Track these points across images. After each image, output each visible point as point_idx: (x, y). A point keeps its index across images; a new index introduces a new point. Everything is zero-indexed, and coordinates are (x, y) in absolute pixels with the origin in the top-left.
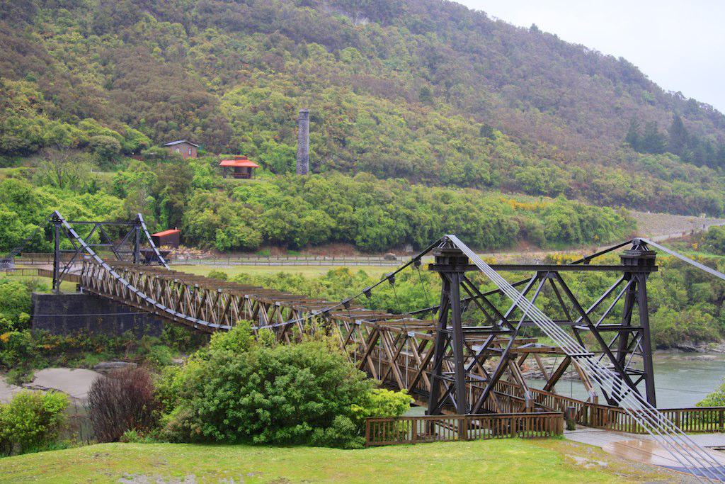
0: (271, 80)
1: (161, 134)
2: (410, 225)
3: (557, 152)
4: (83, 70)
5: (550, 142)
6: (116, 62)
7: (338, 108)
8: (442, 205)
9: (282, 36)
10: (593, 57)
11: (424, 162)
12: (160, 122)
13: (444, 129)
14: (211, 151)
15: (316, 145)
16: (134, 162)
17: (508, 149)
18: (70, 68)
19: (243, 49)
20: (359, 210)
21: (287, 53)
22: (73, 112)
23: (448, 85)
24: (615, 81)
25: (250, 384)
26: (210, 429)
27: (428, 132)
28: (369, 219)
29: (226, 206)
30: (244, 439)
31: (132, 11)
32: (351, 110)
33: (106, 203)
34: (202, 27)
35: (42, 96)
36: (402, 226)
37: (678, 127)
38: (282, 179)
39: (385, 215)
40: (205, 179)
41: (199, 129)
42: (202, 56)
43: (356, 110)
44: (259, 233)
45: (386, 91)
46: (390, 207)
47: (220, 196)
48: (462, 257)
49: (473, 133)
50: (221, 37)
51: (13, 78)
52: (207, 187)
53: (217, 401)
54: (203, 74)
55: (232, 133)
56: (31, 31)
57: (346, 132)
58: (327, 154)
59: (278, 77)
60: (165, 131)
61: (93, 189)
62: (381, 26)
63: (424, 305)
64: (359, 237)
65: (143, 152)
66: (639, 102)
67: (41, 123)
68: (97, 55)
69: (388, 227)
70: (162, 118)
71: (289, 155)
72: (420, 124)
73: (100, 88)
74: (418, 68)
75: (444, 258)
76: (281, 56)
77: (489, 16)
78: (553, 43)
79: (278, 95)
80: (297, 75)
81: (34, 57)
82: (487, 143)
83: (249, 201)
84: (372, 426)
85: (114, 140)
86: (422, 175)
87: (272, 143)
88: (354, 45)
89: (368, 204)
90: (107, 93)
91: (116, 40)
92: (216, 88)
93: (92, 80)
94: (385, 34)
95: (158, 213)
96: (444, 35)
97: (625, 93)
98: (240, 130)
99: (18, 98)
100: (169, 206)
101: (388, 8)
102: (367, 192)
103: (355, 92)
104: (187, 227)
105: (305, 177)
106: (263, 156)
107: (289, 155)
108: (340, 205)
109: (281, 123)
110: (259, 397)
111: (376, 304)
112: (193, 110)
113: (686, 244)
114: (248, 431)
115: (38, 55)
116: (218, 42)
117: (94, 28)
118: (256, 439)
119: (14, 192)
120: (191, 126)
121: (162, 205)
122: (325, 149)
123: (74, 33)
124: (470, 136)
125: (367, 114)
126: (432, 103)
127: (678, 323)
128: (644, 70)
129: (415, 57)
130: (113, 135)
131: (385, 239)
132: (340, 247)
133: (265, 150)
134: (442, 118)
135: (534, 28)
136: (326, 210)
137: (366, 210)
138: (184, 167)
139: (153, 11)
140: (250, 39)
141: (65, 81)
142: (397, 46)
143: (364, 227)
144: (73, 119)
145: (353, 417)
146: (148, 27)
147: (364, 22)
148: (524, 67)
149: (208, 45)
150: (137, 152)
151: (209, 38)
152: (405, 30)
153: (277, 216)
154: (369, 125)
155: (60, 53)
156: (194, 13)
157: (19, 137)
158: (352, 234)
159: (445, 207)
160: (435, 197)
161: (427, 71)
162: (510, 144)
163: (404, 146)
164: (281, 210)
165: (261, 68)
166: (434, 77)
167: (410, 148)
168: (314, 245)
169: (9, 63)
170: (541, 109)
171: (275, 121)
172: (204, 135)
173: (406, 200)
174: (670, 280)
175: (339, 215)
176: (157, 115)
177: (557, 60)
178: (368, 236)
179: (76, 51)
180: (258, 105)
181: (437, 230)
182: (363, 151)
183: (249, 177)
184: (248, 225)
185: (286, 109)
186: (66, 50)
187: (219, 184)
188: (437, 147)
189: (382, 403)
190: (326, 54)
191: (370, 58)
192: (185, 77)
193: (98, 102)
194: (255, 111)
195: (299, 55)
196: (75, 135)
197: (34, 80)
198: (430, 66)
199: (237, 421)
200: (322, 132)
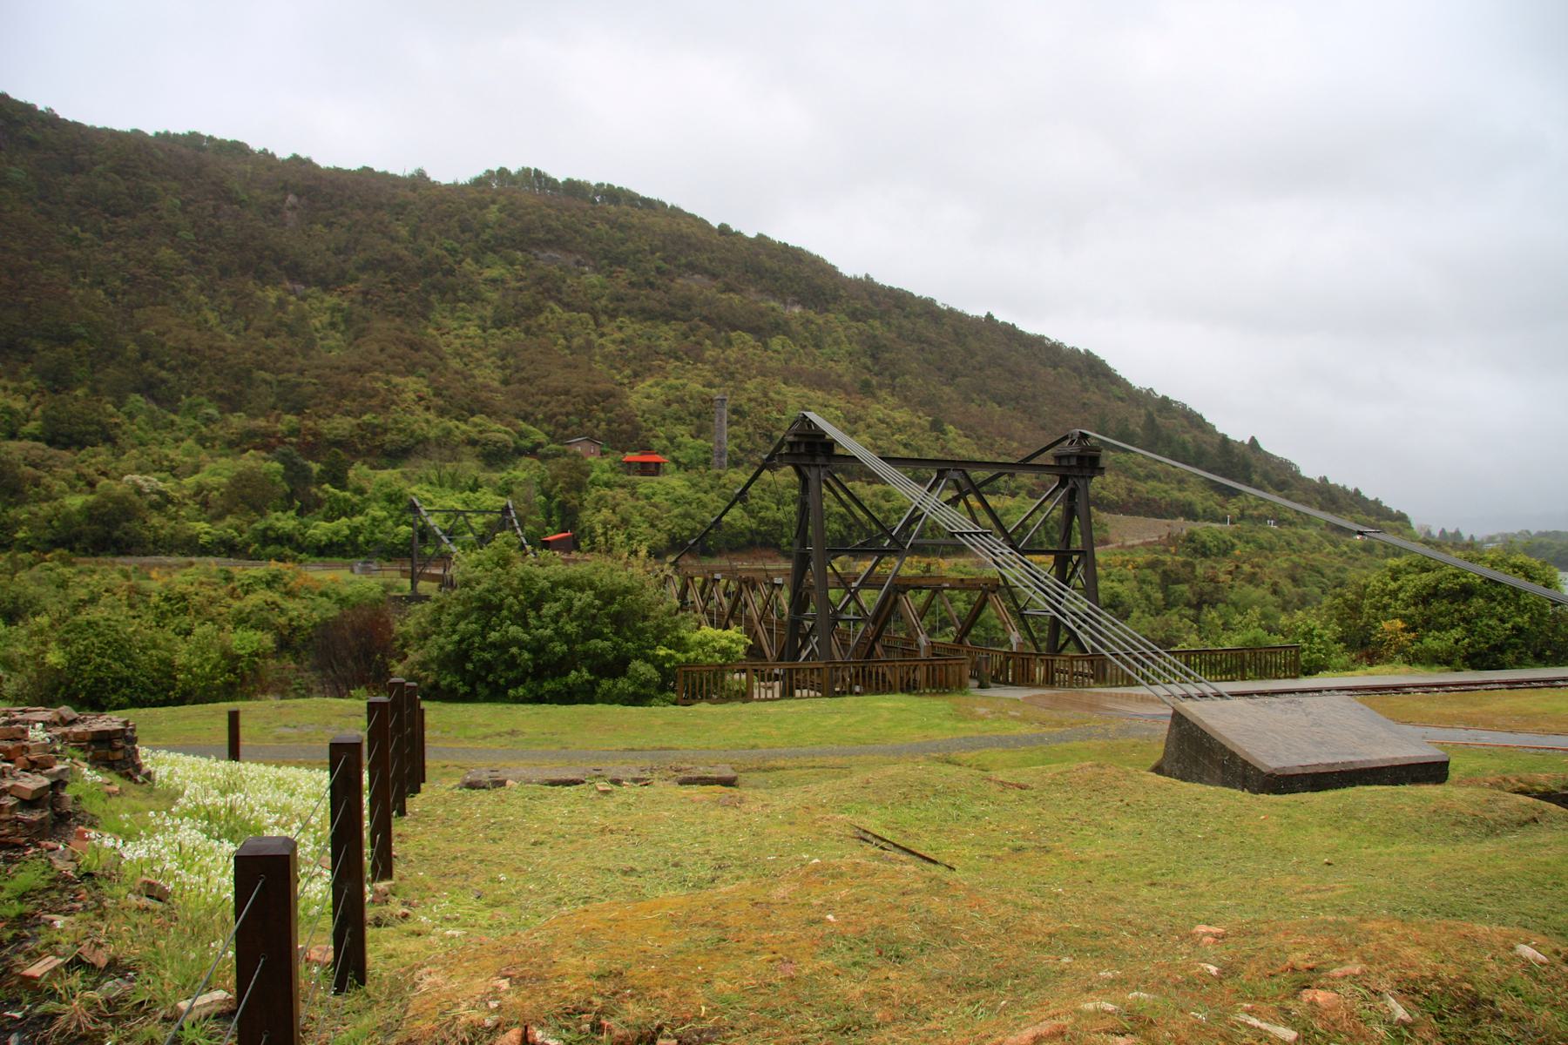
0: (688, 371)
1: (560, 431)
3: (1018, 449)
4: (478, 366)
5: (1010, 438)
6: (515, 355)
7: (764, 400)
8: (882, 503)
9: (702, 324)
10: (1056, 349)
12: (559, 417)
13: (887, 423)
14: (617, 449)
15: (738, 441)
16: (526, 460)
17: (962, 446)
18: (466, 365)
19: (659, 338)
22: (462, 408)
23: (893, 377)
24: (1081, 375)
25: (505, 613)
26: (449, 679)
27: (869, 426)
29: (627, 504)
30: (497, 694)
31: (536, 302)
32: (779, 401)
33: (489, 502)
34: (613, 316)
37: (1150, 423)
38: (693, 475)
40: (605, 477)
41: (603, 425)
42: (611, 348)
43: (785, 402)
44: (665, 536)
45: (820, 381)
47: (620, 494)
48: (822, 444)
49: (922, 428)
50: (632, 327)
51: (402, 375)
52: (607, 485)
53: (456, 637)
54: (611, 367)
55: (641, 428)
56: (426, 327)
58: (752, 451)
60: (566, 427)
61: (475, 487)
65: (539, 450)
66: (1108, 399)
67: (428, 421)
68: (496, 349)
70: (561, 414)
71: (706, 452)
72: (859, 418)
73: (496, 384)
75: (798, 444)
77: (939, 303)
78: (1010, 332)
79: (696, 387)
80: (718, 365)
81: (426, 353)
82: (938, 439)
83: (656, 499)
84: (687, 676)
85: (506, 437)
87: (687, 439)
88: (785, 334)
90: (503, 389)
91: (516, 333)
92: (626, 381)
93: (488, 375)
94: (821, 321)
95: (549, 514)
96: (888, 323)
97: (1092, 388)
98: (651, 425)
99: (404, 395)
100: (562, 505)
101: (824, 294)
104: (583, 531)
105: (721, 472)
106: (676, 454)
107: (706, 452)
108: (761, 503)
109: (698, 417)
110: (514, 630)
112: (598, 404)
113: (1162, 547)
114: (502, 681)
115: (431, 351)
116: (629, 332)
117: (494, 322)
118: (511, 692)
119: (387, 490)
120: (595, 421)
121: (554, 505)
122: (748, 445)
124: (918, 431)
125: (799, 405)
126: (874, 396)
127: (1153, 630)
128: (1111, 363)
129: (856, 347)
130: (506, 432)
133: (678, 447)
134: (886, 411)
135: (989, 317)
138: (580, 462)
139: (559, 301)
140: (666, 328)
141: (459, 377)
142: (835, 335)
145: (658, 664)
147: (797, 310)
148: (979, 358)
149: (618, 336)
150: (533, 451)
151: (620, 329)
152: (843, 317)
153: (686, 515)
155: (456, 349)
156: (604, 302)
157: (402, 437)
159: (887, 506)
160: (875, 495)
161: (869, 362)
162: (965, 440)
164: (693, 509)
165: (678, 359)
166: (877, 368)
168: (732, 550)
169: (398, 360)
170: (1000, 404)
171: (691, 414)
172: (610, 431)
174: (1144, 581)
176: (556, 410)
177: (1016, 351)
179: (472, 346)
180: (671, 397)
183: (656, 473)
184: (653, 526)
185: (704, 401)
186: (463, 346)
188: (880, 443)
189: (701, 644)
190: (752, 343)
191: (804, 347)
192: (590, 370)
193: (492, 398)
194: (668, 404)
195: (722, 344)
196: (464, 432)
197: (423, 376)
198: (873, 356)
199: (488, 666)
200: (746, 426)
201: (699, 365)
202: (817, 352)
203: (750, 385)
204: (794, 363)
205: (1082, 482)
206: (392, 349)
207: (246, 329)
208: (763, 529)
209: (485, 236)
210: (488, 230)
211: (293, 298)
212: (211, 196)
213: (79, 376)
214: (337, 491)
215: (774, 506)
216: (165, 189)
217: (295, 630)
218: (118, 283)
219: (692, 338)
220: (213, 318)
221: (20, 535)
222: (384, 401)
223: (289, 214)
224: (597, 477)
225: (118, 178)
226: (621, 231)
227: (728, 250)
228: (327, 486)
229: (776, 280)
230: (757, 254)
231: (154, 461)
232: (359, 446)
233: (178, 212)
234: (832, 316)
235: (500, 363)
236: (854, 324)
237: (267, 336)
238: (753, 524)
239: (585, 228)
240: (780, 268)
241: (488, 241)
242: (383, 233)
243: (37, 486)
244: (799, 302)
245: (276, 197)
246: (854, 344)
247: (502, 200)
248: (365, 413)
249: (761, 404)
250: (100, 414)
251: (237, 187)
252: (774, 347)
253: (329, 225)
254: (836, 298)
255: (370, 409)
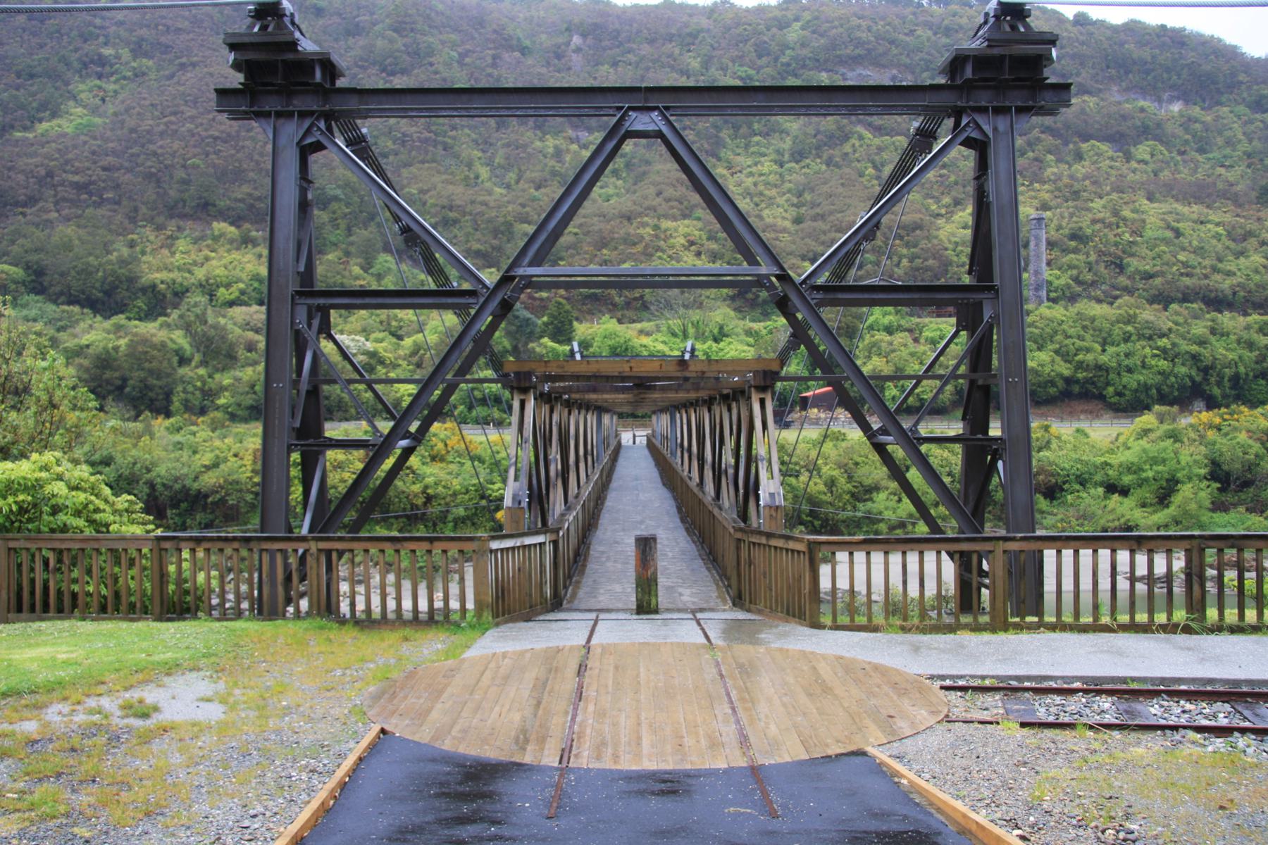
2: (1199, 369)
6: (812, 190)
7: (1114, 220)
9: (1043, 136)
11: (1252, 285)
15: (1075, 272)
18: (757, 205)
20: (1111, 350)
21: (1050, 157)
28: (1126, 362)
32: (1134, 221)
35: (704, 237)
36: (1183, 370)
39: (1155, 356)
41: (905, 262)
43: (1144, 221)
46: (1164, 342)
51: (674, 219)
54: (928, 196)
55: (950, 263)
57: (1124, 252)
59: (1033, 190)
62: (1203, 109)
63: (1166, 476)
64: (1111, 389)
69: (1159, 373)
72: (1249, 234)
73: (787, 224)
74: (1262, 160)
76: (1041, 162)
80: (1060, 184)
86: (1249, 305)
89: (1127, 339)
91: (817, 165)
92: (943, 211)
94: (1209, 118)
99: (672, 241)
101: (1214, 83)
102: (1128, 322)
103: (1149, 199)
108: (1079, 343)
111: (1086, 476)
117: (792, 155)
120: (895, 259)
122: (1089, 277)
123: (767, 164)
125: (1162, 224)
131: (1154, 391)
132: (1078, 406)
136: (1057, 352)
137: (1123, 348)
142: (1228, 133)
143: (1119, 374)
144: (735, 259)
146: (861, 146)
147: (1176, 107)
152: (1242, 109)
154: (1164, 239)
158: (1099, 384)
163: (1220, 265)
167: (1228, 268)
169: (675, 204)
173: (1193, 331)
175: (1077, 358)
178: (1125, 387)
179: (767, 184)
181: (1247, 374)
182: (1148, 276)
187: (907, 326)
190: (1110, 153)
191: (1182, 153)
197: (699, 219)
200: (1088, 255)
201: (1037, 185)
202: (1200, 158)
203: (1097, 204)
204: (1166, 175)
205: (1002, 123)
206: (670, 192)
207: (517, 182)
208: (1081, 375)
209: (784, 59)
210: (788, 52)
211: (574, 147)
212: (491, 46)
213: (333, 239)
214: (555, 345)
215: (1098, 347)
216: (443, 43)
217: (429, 499)
218: (389, 143)
219: (1031, 154)
220: (484, 172)
221: (222, 401)
222: (646, 246)
223: (574, 56)
224: (876, 321)
225: (395, 35)
226: (947, 36)
227: (1083, 43)
228: (545, 340)
229: (1148, 72)
230: (1122, 44)
231: (381, 322)
232: (617, 299)
233: (455, 65)
234: (1226, 109)
235: (795, 200)
236: (1258, 116)
237: (538, 188)
238: (1065, 369)
239: (901, 37)
240: (1153, 57)
241: (788, 65)
242: (673, 68)
243: (250, 350)
244: (1178, 99)
245: (560, 40)
246: (1256, 143)
247: (807, 16)
248: (624, 262)
249: (1109, 226)
250: (344, 277)
251: (519, 33)
252: (1140, 157)
253: (615, 64)
254: (1233, 86)
255: (630, 257)
